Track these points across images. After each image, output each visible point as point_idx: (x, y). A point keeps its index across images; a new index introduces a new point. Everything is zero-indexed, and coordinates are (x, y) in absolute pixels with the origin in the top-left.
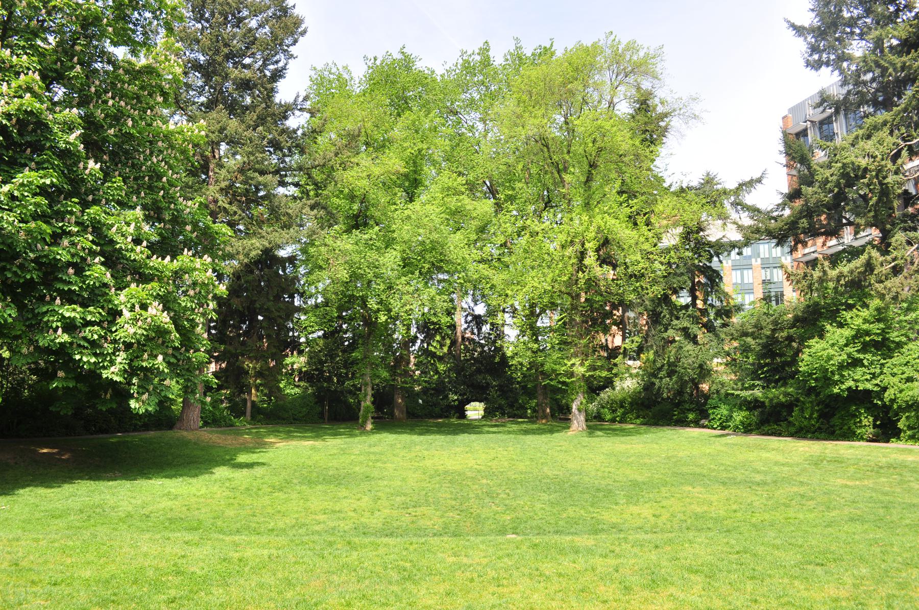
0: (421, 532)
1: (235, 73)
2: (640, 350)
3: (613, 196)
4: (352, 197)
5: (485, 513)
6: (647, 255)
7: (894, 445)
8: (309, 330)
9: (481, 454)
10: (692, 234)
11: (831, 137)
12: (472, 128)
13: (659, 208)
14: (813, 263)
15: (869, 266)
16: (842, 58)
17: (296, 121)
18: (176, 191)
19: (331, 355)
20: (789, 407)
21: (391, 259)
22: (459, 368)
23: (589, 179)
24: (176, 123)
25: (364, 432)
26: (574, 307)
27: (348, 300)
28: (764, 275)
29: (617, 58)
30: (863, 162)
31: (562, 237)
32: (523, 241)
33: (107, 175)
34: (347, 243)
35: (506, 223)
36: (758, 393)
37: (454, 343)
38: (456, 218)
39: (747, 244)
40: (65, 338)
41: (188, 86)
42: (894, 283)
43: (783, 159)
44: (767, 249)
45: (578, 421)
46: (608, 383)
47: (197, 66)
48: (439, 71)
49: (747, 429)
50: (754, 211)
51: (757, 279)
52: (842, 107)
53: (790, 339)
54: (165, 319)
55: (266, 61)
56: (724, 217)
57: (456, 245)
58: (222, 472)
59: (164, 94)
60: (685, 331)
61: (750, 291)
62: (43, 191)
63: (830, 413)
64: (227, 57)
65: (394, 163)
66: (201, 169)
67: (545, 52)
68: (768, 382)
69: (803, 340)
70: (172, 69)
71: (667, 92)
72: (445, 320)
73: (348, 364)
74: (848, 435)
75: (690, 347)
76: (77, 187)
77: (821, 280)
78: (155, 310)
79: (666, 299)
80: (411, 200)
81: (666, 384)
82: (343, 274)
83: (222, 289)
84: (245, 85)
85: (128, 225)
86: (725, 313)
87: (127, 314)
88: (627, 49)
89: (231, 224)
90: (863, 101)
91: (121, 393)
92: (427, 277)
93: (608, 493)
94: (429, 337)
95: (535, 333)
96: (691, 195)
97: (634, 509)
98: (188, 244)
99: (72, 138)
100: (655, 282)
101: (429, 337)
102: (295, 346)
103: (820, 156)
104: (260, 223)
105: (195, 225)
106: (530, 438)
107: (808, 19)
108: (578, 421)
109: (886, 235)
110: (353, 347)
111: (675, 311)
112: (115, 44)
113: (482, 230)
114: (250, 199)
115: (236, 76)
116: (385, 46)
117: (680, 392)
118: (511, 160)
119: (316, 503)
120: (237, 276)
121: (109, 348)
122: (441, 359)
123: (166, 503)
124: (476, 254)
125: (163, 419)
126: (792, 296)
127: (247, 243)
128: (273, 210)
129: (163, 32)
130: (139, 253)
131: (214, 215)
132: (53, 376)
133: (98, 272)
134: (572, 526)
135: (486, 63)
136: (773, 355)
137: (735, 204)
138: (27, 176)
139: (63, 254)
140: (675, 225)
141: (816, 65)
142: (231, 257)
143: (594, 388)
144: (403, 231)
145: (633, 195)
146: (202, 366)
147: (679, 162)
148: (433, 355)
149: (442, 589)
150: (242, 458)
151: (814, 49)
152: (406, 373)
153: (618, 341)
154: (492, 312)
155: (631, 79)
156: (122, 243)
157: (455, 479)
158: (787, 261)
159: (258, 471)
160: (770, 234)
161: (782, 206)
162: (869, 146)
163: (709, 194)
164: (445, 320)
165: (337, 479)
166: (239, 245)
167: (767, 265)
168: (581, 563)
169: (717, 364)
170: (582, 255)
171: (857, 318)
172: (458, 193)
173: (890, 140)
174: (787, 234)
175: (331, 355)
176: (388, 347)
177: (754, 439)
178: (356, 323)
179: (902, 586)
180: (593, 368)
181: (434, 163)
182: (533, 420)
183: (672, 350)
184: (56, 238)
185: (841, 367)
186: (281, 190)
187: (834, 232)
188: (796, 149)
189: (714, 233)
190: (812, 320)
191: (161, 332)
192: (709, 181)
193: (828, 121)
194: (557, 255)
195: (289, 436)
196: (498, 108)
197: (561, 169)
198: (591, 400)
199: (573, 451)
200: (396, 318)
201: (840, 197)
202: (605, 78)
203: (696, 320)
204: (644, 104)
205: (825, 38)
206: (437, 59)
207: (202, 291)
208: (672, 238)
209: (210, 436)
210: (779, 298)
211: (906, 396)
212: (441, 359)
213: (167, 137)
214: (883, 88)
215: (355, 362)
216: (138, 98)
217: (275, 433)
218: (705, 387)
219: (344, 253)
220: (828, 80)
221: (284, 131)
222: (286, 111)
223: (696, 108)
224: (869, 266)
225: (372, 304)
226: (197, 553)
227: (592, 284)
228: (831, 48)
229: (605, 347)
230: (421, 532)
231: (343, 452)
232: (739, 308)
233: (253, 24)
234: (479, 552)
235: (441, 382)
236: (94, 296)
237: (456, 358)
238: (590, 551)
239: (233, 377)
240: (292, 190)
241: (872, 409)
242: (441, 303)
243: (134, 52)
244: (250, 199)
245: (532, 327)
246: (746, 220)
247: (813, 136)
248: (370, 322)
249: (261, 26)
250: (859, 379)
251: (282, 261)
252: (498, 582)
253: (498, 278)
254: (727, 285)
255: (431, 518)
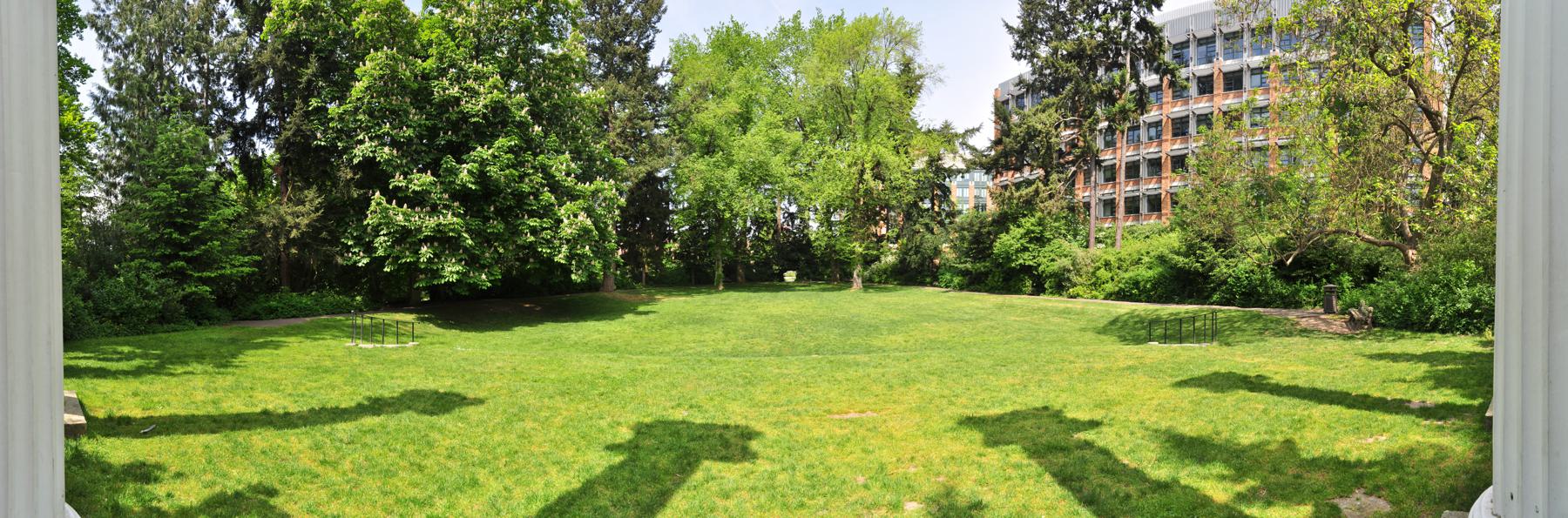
0: (756, 354)
1: (620, 49)
2: (898, 237)
3: (884, 131)
4: (704, 133)
5: (797, 341)
6: (904, 174)
7: (1042, 297)
8: (679, 225)
9: (795, 305)
10: (934, 161)
11: (1022, 107)
12: (786, 79)
13: (914, 142)
14: (1005, 187)
15: (1037, 192)
16: (1034, 55)
17: (664, 80)
18: (589, 139)
19: (695, 242)
20: (986, 274)
21: (731, 175)
22: (779, 248)
23: (868, 119)
24: (586, 91)
25: (718, 291)
26: (856, 208)
27: (704, 205)
28: (976, 192)
29: (891, 29)
30: (1039, 127)
31: (849, 160)
32: (823, 161)
33: (546, 135)
34: (701, 165)
35: (811, 148)
36: (969, 266)
37: (776, 232)
38: (776, 144)
39: (967, 171)
40: (532, 239)
41: (590, 64)
42: (1049, 203)
43: (993, 117)
44: (979, 176)
45: (857, 282)
46: (877, 258)
47: (594, 49)
48: (763, 35)
49: (961, 288)
50: (973, 149)
51: (971, 194)
52: (1031, 88)
53: (989, 233)
54: (589, 222)
55: (641, 36)
56: (954, 152)
57: (777, 164)
58: (629, 317)
59: (576, 73)
60: (926, 225)
61: (967, 202)
62: (510, 150)
63: (1005, 277)
64: (614, 39)
65: (732, 106)
66: (604, 121)
67: (839, 20)
68: (975, 259)
69: (997, 234)
70: (580, 53)
71: (924, 59)
72: (769, 216)
73: (706, 247)
74: (1018, 292)
75: (928, 236)
76: (530, 145)
77: (1010, 198)
78: (582, 217)
79: (915, 204)
80: (745, 133)
81: (914, 259)
82: (700, 187)
83: (622, 201)
84: (627, 58)
85: (562, 165)
86: (952, 215)
87: (566, 221)
88: (898, 23)
89: (626, 157)
90: (1043, 88)
91: (566, 270)
92: (756, 186)
93: (877, 328)
94: (759, 228)
95: (831, 225)
96: (935, 135)
97: (893, 338)
98: (599, 173)
99: (523, 113)
100: (909, 193)
101: (759, 228)
102: (671, 236)
103: (1015, 119)
104: (644, 155)
105: (602, 161)
106: (826, 294)
107: (1016, 23)
108: (857, 282)
109: (1048, 174)
110: (708, 236)
111: (922, 212)
112: (542, 43)
113: (794, 153)
114: (636, 139)
115: (623, 56)
116: (720, 19)
117: (922, 265)
118: (814, 103)
119: (688, 336)
120: (631, 191)
121: (557, 242)
122: (767, 242)
123: (596, 336)
124: (790, 170)
125: (592, 285)
126: (992, 207)
127: (636, 169)
128: (652, 145)
129: (570, 27)
130: (570, 181)
131: (614, 152)
132: (527, 262)
133: (548, 196)
134: (854, 349)
135: (798, 28)
136: (979, 241)
137: (962, 144)
138: (501, 142)
139: (526, 188)
140: (924, 155)
141: (1018, 57)
142: (626, 179)
143: (868, 261)
144: (739, 155)
145: (897, 133)
146: (613, 252)
147: (928, 111)
148: (762, 240)
149: (770, 390)
150: (641, 309)
151: (1018, 46)
152: (744, 252)
153: (884, 231)
154: (801, 210)
155: (899, 47)
156: (560, 176)
157: (777, 320)
158: (990, 184)
159: (651, 316)
160: (982, 166)
161: (990, 149)
162: (1043, 116)
163: (946, 135)
164: (769, 216)
165: (701, 321)
166: (630, 171)
167: (979, 186)
168: (861, 372)
169: (945, 247)
170: (862, 172)
171: (1028, 222)
172: (778, 127)
173: (1056, 115)
174: (993, 166)
175: (695, 242)
176: (732, 235)
177: (965, 294)
178: (710, 216)
179: (1045, 374)
180: (867, 248)
181: (761, 105)
182: (828, 282)
183: (918, 237)
184: (521, 178)
185: (1017, 251)
186: (656, 131)
187: (1019, 169)
188: (1001, 113)
189: (948, 162)
190: (1003, 222)
191: (586, 231)
192: (947, 126)
193: (1020, 97)
194: (846, 172)
195: (670, 295)
196: (806, 63)
197: (849, 110)
198: (865, 269)
199: (855, 302)
200: (737, 215)
201: (1024, 147)
202: (881, 44)
203: (933, 219)
204: (907, 67)
205: (1026, 37)
206: (760, 27)
207: (610, 204)
208: (920, 164)
209: (620, 295)
210: (984, 207)
211: (1050, 270)
212: (767, 242)
213: (581, 102)
214: (1055, 81)
215: (710, 245)
216: (560, 78)
217: (660, 292)
218: (937, 261)
219: (700, 172)
220: (1024, 68)
221: (657, 88)
222: (657, 72)
223: (942, 74)
224: (1037, 192)
225: (721, 206)
226: (617, 366)
227: (868, 192)
228: (1027, 47)
229: (875, 235)
230: (756, 354)
231: (705, 304)
232: (960, 212)
233: (629, 10)
234: (794, 367)
235: (767, 258)
236: (547, 211)
237: (777, 241)
238: (866, 364)
239: (632, 258)
240: (664, 130)
241: (1032, 276)
242: (767, 204)
243: (554, 47)
244: (636, 139)
245: (828, 220)
246: (968, 155)
247: (1012, 105)
248: (720, 220)
249: (635, 10)
250: (1026, 259)
251: (660, 180)
252: (807, 385)
253: (806, 187)
254: (953, 198)
255: (763, 345)
